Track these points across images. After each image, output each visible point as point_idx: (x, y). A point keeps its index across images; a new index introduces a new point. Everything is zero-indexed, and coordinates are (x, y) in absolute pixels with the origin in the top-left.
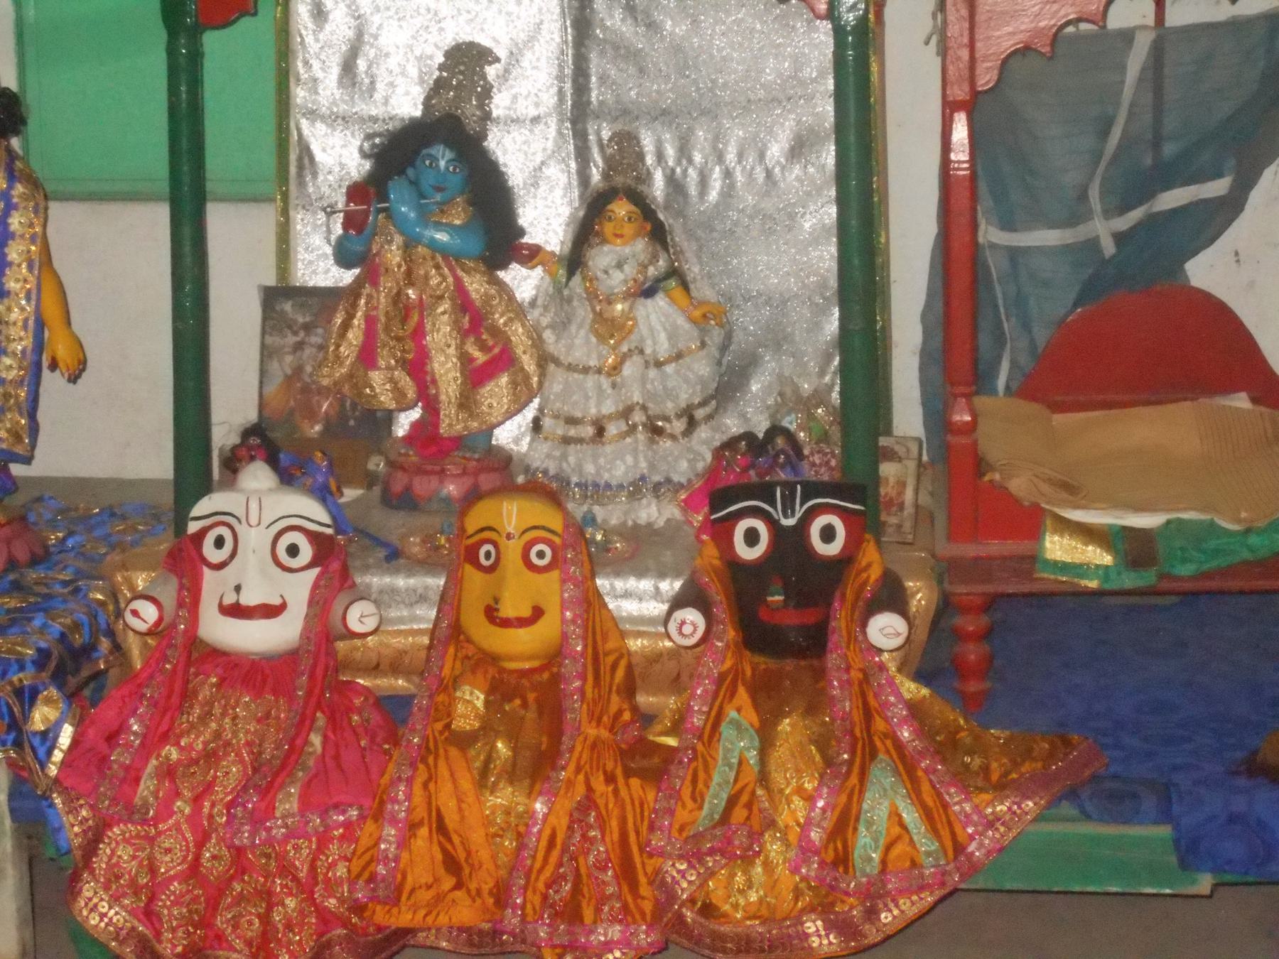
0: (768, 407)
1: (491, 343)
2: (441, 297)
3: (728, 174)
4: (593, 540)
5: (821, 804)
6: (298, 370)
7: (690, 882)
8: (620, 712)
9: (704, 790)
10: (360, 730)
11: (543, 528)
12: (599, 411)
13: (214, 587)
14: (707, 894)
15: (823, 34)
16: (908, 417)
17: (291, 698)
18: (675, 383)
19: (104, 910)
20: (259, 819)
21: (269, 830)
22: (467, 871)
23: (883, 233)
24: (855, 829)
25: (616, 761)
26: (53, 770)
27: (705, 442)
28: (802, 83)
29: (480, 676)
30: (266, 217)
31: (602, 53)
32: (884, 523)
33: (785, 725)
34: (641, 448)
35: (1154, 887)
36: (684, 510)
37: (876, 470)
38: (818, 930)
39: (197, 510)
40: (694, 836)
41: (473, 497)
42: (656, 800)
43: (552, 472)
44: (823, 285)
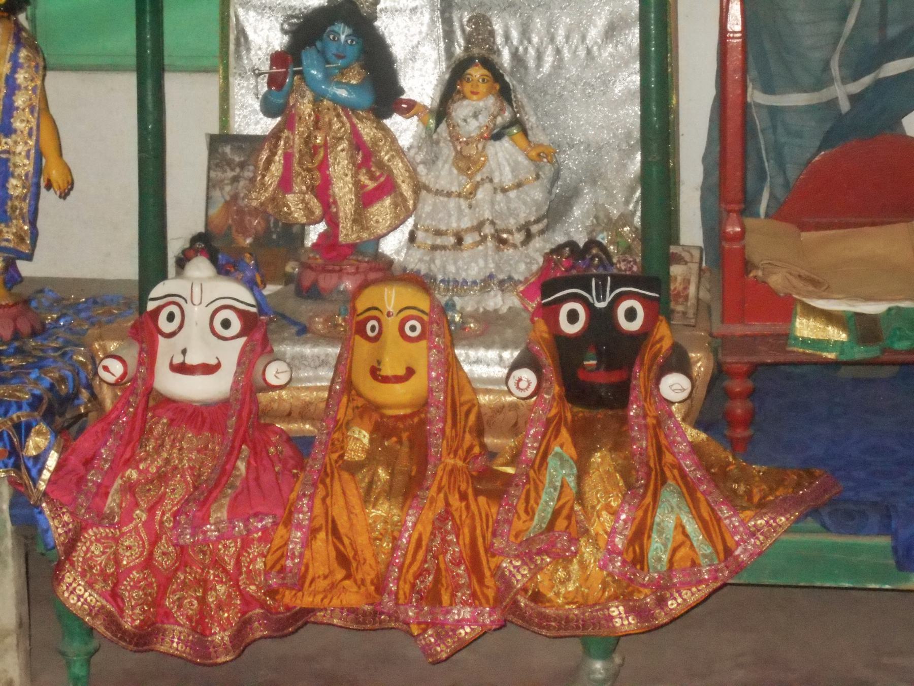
2: (341, 139)
3: (558, 51)
4: (453, 322)
5: (623, 517)
6: (235, 197)
7: (523, 575)
8: (470, 448)
9: (535, 506)
10: (275, 459)
13: (166, 351)
14: (537, 584)
16: (691, 231)
17: (224, 433)
19: (81, 593)
20: (197, 526)
21: (205, 533)
22: (354, 565)
23: (674, 96)
24: (649, 537)
25: (468, 483)
26: (42, 486)
29: (366, 420)
30: (213, 83)
32: (673, 311)
33: (597, 457)
34: (490, 253)
35: (875, 583)
36: (521, 299)
38: (620, 613)
39: (154, 293)
40: (527, 540)
42: (498, 514)
44: (629, 135)
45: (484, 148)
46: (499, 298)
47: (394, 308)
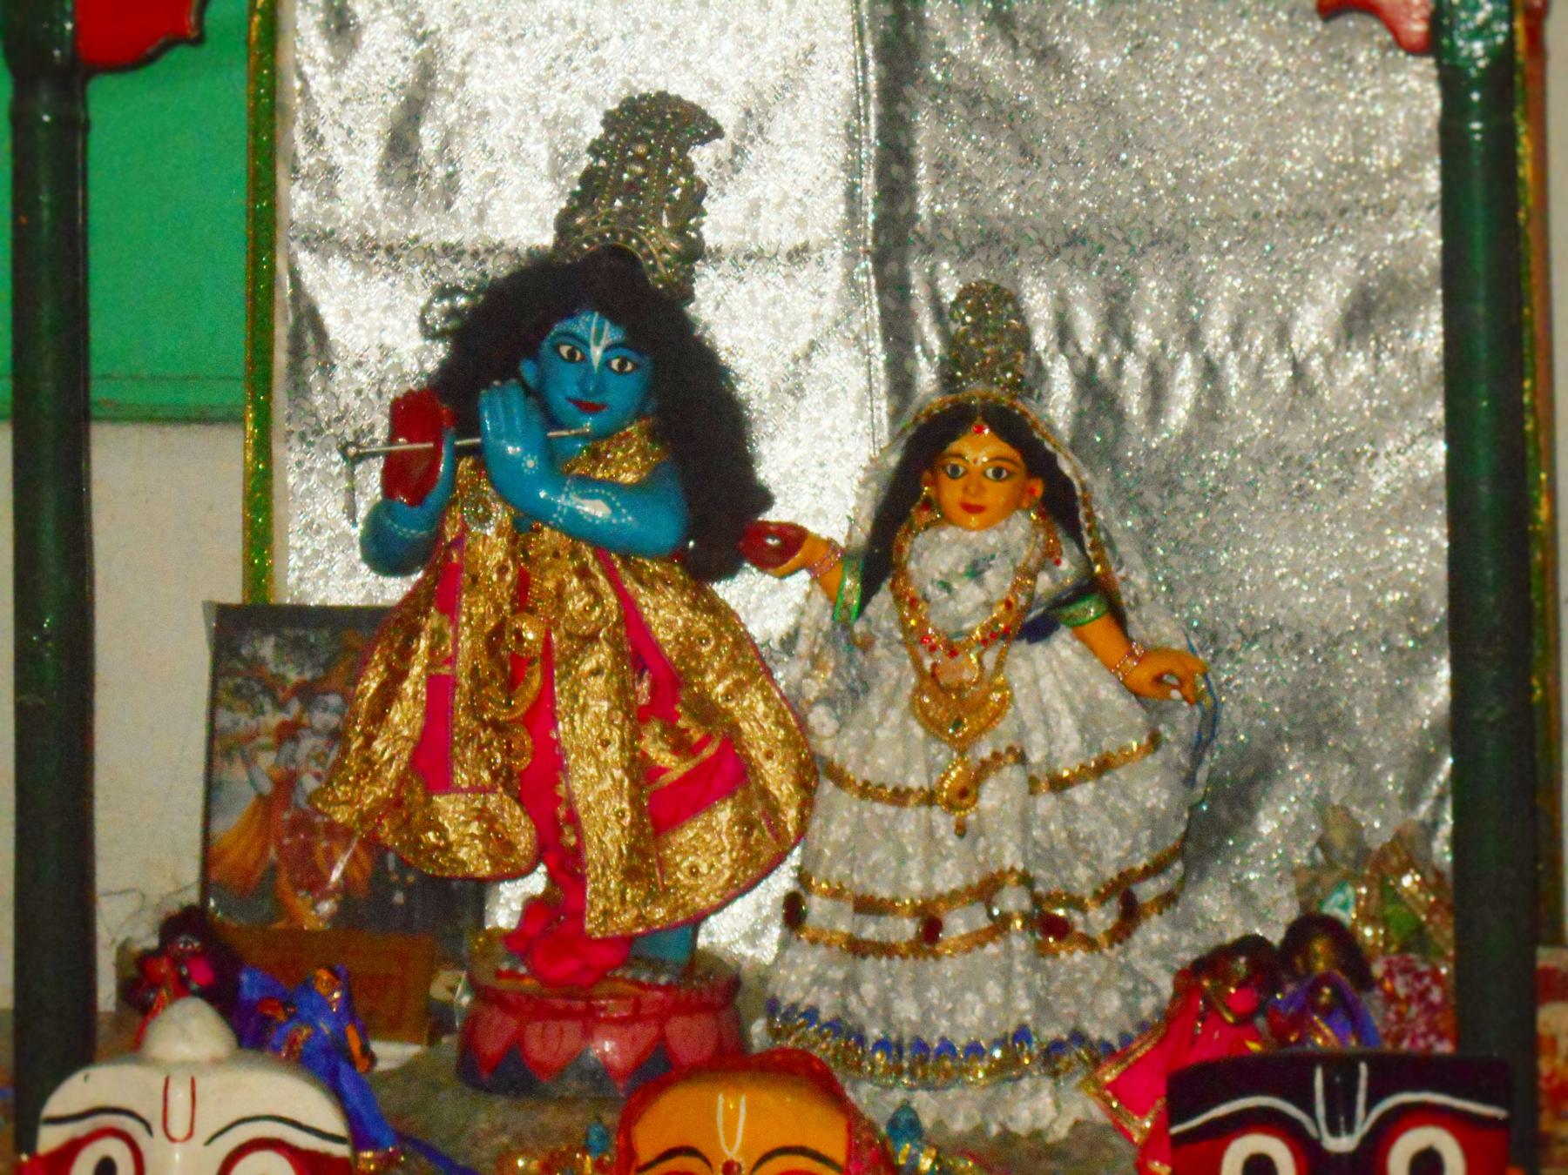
0: (1295, 873)
1: (696, 735)
2: (592, 638)
3: (1210, 371)
6: (287, 783)
11: (801, 1151)
12: (929, 887)
15: (1419, 85)
18: (1094, 826)
23: (1544, 501)
27: (1156, 954)
28: (1372, 181)
30: (222, 457)
31: (941, 113)
34: (1019, 968)
37: (1532, 1019)
39: (58, 1104)
41: (655, 1075)
43: (825, 1016)
44: (1414, 608)
45: (1000, 665)
46: (1045, 1101)
47: (744, 1151)
